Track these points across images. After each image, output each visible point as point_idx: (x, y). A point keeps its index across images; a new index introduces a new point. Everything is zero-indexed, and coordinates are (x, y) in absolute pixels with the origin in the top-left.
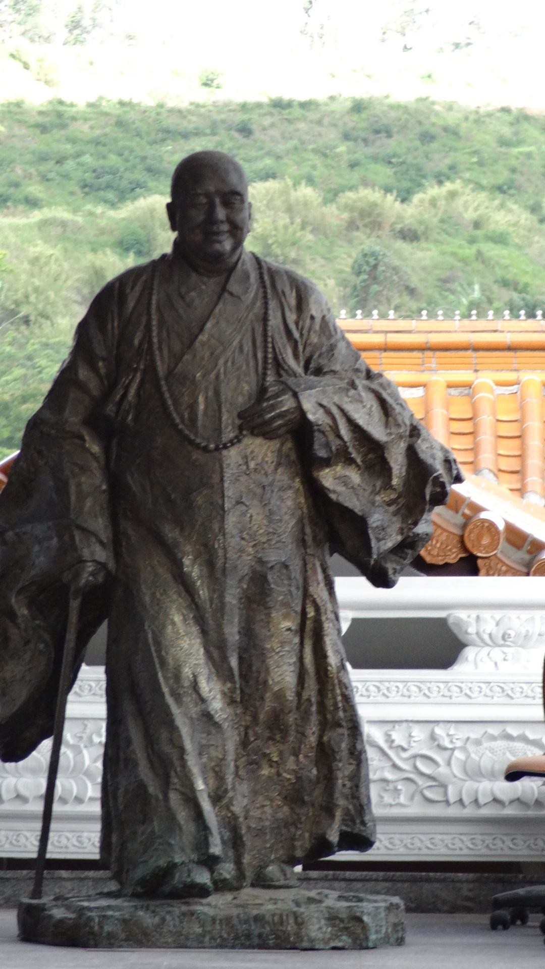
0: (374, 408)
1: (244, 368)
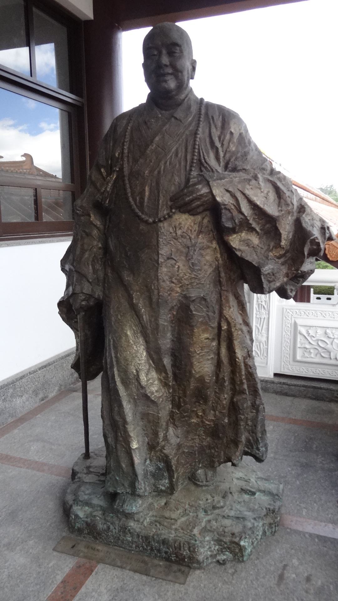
0: (270, 194)
1: (177, 166)
